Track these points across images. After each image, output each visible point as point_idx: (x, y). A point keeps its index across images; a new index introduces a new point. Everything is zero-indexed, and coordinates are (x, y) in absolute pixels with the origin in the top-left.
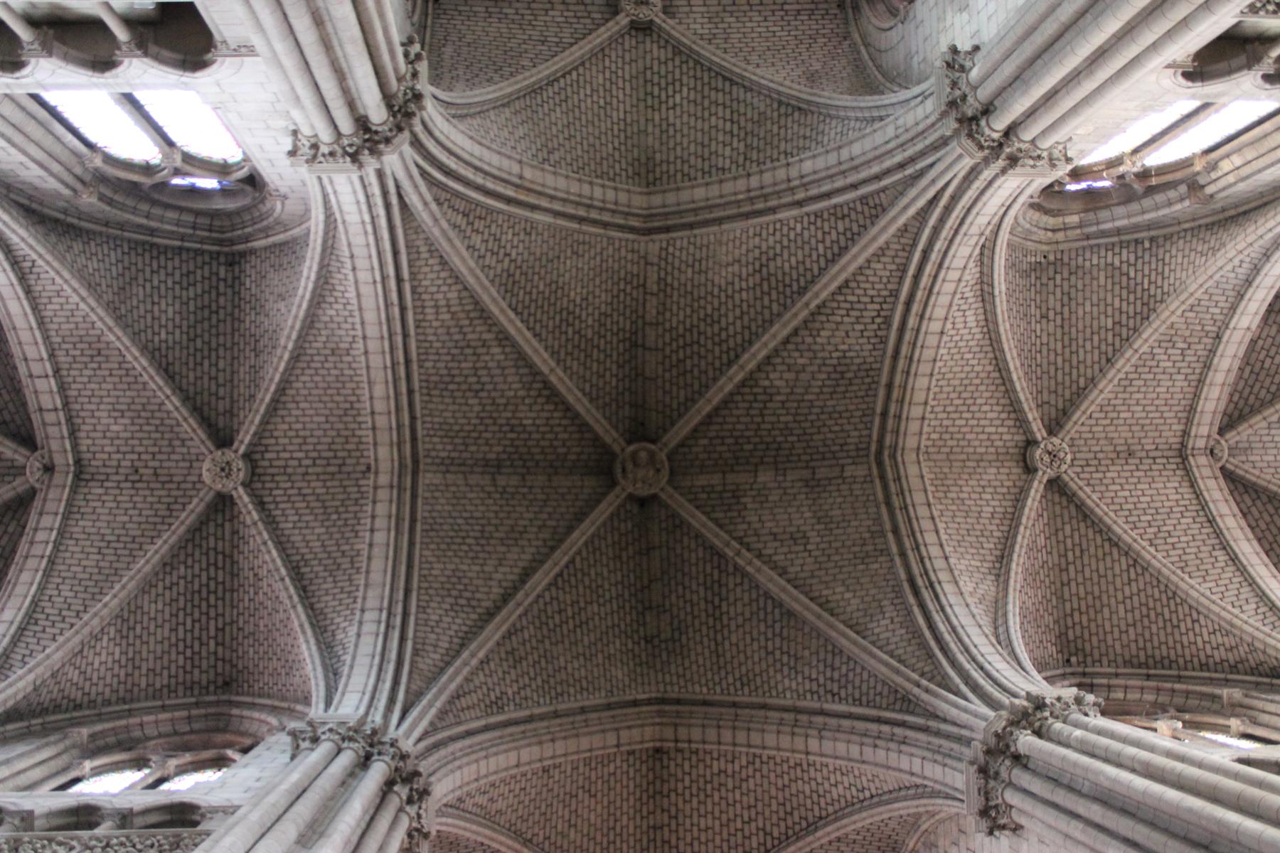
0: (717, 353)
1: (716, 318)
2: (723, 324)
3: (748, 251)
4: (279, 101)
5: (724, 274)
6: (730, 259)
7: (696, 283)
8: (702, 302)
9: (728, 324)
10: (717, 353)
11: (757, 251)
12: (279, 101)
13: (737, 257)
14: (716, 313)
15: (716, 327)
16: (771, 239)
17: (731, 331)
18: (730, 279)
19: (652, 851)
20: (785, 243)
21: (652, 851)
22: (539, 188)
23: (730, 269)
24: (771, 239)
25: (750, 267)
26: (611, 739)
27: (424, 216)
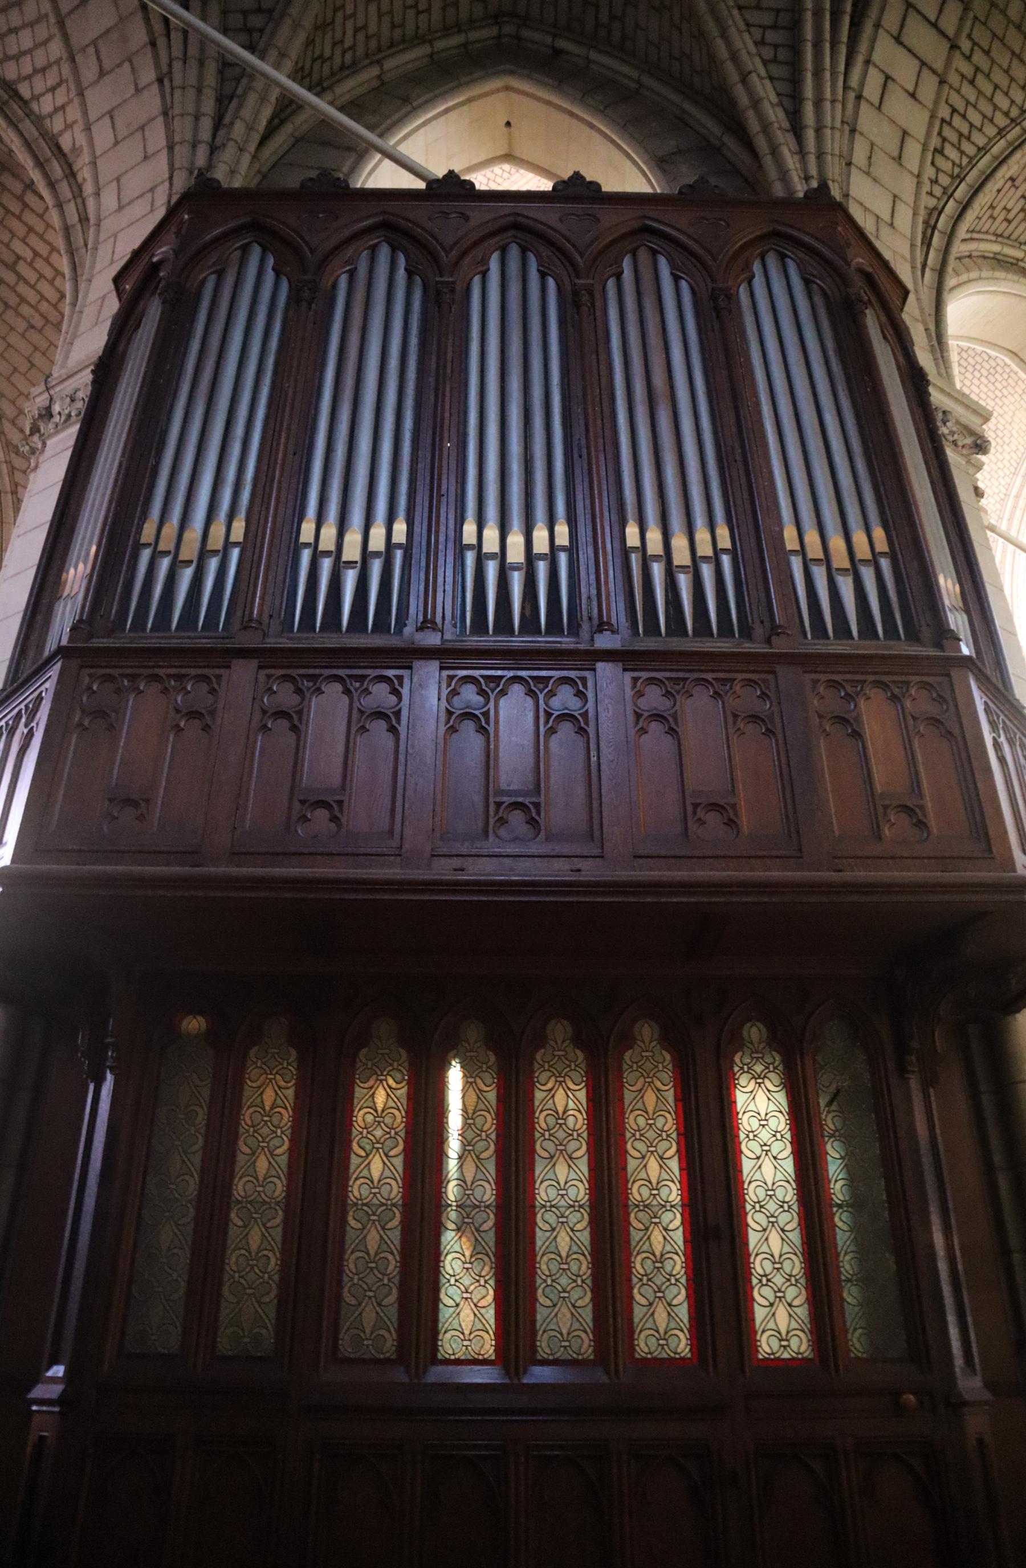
0: (970, 360)
1: (990, 377)
2: (983, 379)
3: (1012, 435)
4: (975, 18)
5: (1011, 406)
6: (1016, 419)
7: (1020, 382)
8: (1006, 376)
9: (981, 383)
10: (970, 360)
11: (1007, 441)
12: (975, 18)
13: (1013, 424)
14: (993, 380)
15: (985, 373)
16: (1008, 457)
17: (975, 381)
18: (1004, 407)
19: (398, 4)
20: (999, 464)
21: (398, 4)
22: (984, 177)
23: (1010, 414)
24: (1008, 457)
25: (1002, 428)
26: (453, 1199)
27: (767, 91)
